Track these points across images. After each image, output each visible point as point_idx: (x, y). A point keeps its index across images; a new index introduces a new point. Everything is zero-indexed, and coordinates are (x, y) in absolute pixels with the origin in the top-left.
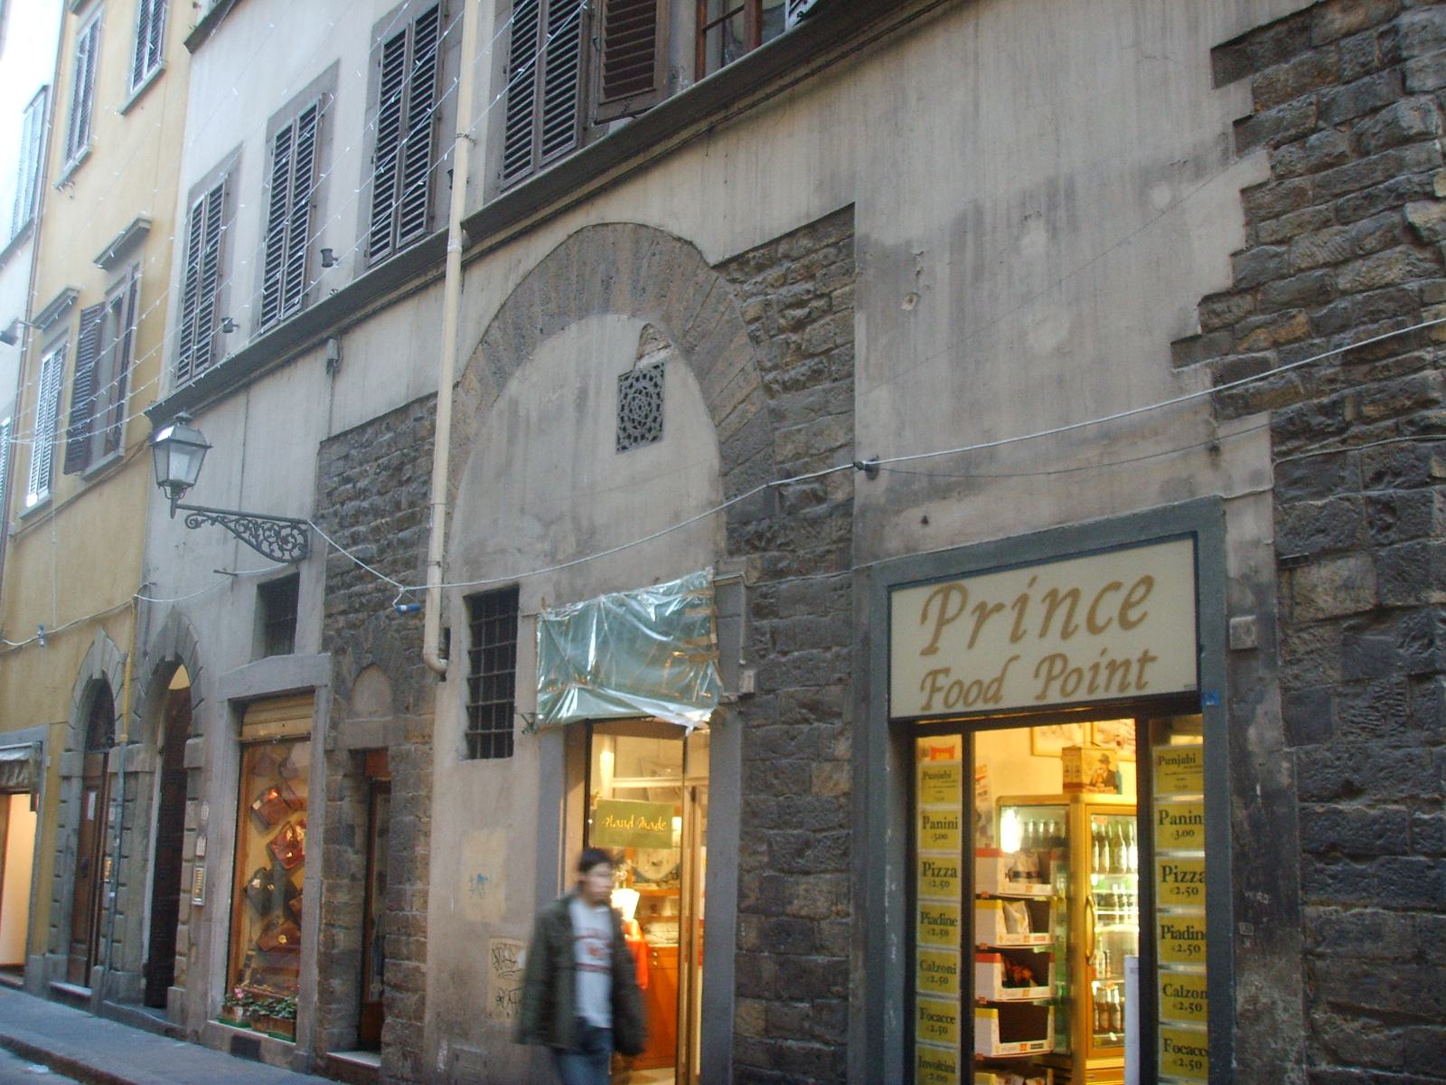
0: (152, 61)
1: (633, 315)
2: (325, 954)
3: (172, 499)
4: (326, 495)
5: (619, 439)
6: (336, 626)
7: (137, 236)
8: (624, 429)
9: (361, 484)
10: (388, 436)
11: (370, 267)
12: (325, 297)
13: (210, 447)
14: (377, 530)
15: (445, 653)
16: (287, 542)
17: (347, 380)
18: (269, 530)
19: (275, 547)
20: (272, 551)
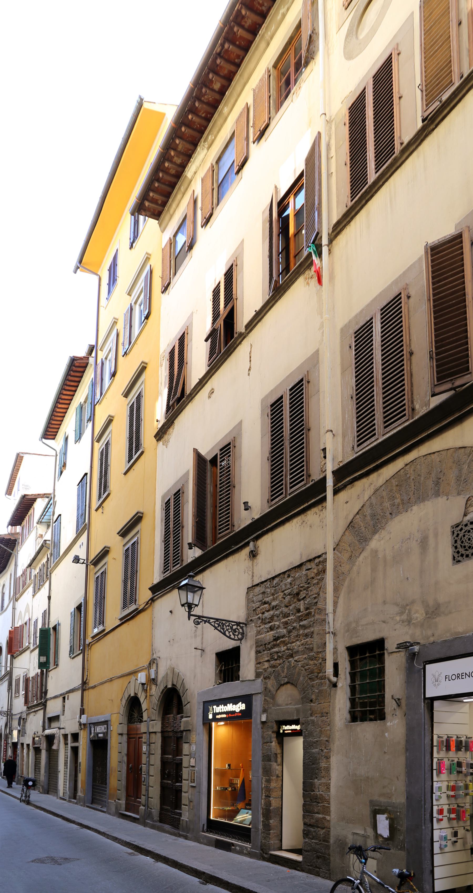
0: (105, 492)
1: (459, 494)
2: (266, 809)
3: (188, 612)
4: (252, 611)
5: (454, 557)
6: (264, 667)
7: (137, 520)
8: (458, 552)
9: (274, 603)
10: (289, 580)
11: (271, 506)
12: (189, 560)
13: (205, 588)
14: (286, 623)
15: (336, 674)
16: (236, 632)
17: (260, 558)
18: (228, 626)
19: (231, 633)
20: (230, 635)
